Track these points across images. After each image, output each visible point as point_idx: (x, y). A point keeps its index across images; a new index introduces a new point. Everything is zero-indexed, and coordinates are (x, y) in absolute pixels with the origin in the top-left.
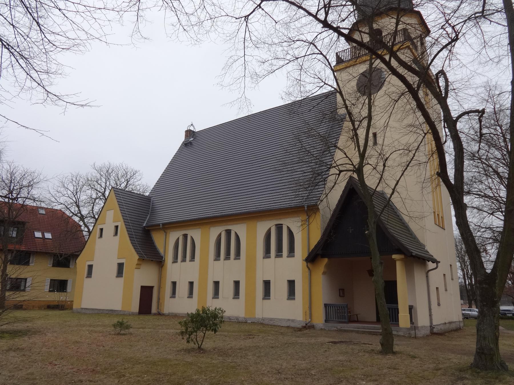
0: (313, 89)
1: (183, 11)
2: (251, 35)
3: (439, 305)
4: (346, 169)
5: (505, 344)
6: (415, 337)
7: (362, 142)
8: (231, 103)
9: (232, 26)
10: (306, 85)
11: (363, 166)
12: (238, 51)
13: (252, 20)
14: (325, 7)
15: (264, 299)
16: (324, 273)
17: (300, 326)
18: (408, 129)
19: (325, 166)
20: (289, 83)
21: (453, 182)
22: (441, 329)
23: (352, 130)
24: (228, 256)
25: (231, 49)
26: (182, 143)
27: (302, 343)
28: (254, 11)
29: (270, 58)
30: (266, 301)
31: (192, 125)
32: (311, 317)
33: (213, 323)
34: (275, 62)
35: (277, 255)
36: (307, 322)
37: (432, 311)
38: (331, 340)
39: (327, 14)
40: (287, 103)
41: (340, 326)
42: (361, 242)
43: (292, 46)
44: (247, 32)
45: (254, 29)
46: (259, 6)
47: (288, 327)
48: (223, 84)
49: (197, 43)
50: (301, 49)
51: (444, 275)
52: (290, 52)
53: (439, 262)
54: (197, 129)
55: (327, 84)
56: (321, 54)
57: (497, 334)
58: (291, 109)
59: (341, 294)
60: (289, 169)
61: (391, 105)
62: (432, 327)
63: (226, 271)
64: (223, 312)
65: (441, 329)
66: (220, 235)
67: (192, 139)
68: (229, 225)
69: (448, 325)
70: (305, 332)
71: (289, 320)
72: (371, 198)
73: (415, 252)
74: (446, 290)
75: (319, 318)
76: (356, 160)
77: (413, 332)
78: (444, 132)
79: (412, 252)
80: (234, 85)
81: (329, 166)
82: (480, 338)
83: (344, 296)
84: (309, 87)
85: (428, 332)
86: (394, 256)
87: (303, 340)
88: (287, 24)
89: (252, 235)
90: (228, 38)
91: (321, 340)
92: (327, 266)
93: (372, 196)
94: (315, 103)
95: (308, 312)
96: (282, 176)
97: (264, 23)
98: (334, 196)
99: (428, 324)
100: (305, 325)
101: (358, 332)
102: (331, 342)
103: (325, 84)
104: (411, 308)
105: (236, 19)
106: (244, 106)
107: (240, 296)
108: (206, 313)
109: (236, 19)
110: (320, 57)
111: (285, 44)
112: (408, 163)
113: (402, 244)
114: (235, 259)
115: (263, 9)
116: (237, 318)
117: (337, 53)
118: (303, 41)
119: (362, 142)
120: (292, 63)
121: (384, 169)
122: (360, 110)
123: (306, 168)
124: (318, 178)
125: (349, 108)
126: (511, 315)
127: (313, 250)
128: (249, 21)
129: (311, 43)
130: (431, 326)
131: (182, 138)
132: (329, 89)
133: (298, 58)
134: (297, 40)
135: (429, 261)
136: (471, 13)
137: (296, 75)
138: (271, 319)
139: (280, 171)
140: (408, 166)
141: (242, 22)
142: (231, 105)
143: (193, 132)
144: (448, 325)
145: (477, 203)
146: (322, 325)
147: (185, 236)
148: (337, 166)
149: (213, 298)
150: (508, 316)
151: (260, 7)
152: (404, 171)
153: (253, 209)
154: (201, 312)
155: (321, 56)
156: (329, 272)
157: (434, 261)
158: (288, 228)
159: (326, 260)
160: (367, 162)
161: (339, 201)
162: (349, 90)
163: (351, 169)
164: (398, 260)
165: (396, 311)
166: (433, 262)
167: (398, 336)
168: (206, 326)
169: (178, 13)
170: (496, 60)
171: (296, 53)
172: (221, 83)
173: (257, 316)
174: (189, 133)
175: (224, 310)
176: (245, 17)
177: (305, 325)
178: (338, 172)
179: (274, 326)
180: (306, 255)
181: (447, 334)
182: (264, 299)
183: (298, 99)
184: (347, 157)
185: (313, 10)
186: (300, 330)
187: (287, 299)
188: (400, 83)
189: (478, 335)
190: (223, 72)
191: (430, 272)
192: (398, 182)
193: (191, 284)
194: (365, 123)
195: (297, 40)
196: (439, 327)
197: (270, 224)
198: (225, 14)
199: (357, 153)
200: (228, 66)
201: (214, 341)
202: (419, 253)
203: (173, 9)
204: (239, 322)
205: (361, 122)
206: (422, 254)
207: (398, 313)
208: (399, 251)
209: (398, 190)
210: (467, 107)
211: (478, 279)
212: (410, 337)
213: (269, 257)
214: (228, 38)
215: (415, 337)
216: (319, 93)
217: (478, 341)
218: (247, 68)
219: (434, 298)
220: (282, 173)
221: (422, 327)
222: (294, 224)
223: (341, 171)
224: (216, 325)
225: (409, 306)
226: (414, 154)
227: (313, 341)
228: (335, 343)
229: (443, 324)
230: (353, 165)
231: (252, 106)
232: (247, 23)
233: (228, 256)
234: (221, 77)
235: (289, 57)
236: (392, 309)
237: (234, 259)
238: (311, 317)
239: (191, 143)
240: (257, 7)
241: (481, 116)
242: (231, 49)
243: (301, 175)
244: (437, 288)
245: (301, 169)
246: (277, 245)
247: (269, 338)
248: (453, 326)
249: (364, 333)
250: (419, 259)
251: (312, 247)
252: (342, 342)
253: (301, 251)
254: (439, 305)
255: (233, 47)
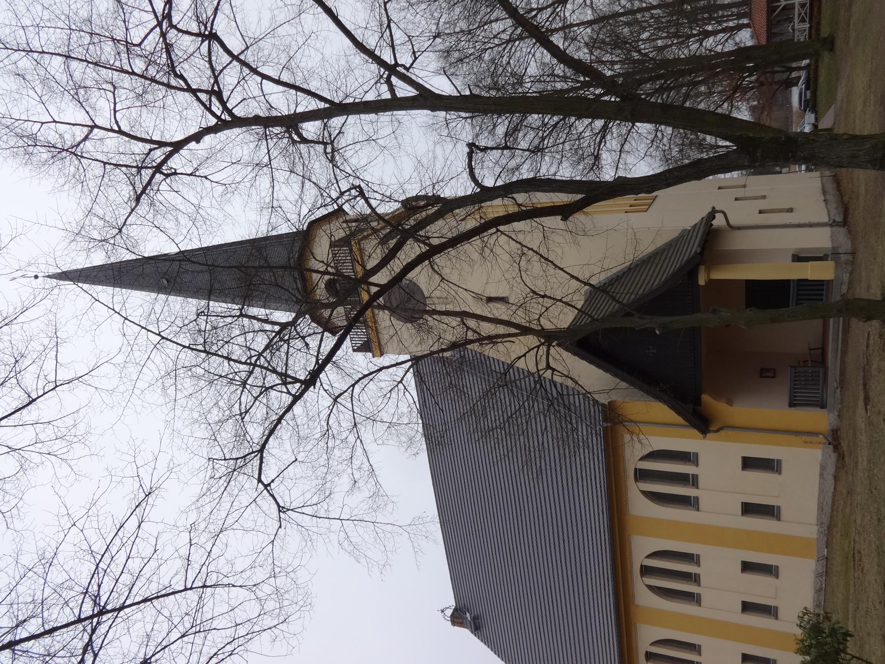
0: (405, 404)
1: (255, 620)
2: (309, 503)
3: (791, 210)
4: (544, 356)
5: (862, 111)
6: (853, 253)
7: (501, 330)
8: (416, 552)
9: (292, 537)
10: (400, 412)
11: (543, 329)
12: (333, 529)
13: (287, 499)
14: (285, 383)
15: (778, 518)
16: (730, 403)
17: (833, 457)
18: (487, 254)
19: (537, 392)
20: (391, 442)
21: (579, 197)
22: (836, 208)
23: (481, 344)
24: (694, 578)
25: (327, 540)
26: (472, 636)
27: (869, 461)
28: (273, 496)
29: (349, 470)
30: (784, 514)
31: (442, 611)
32: (816, 434)
33: (830, 635)
34: (356, 463)
35: (693, 485)
36: (824, 441)
37: (803, 221)
38: (861, 403)
39: (296, 380)
40: (425, 446)
41: (832, 383)
42: (677, 336)
43: (335, 432)
44: (304, 510)
45: (301, 499)
46: (266, 486)
47: (836, 478)
48: (382, 563)
49: (309, 600)
50: (343, 418)
51: (736, 199)
52: (344, 435)
53: (714, 208)
54: (451, 602)
55: (402, 379)
56: (353, 385)
57: (845, 137)
58: (436, 441)
59: (771, 374)
60: (537, 455)
61: (447, 288)
62: (833, 224)
63: (722, 582)
64: (806, 612)
65: (836, 208)
66: (650, 587)
67: (468, 615)
68: (632, 567)
69: (828, 197)
70: (845, 448)
71: (821, 475)
72: (597, 320)
73: (696, 248)
74: (764, 197)
75: (819, 419)
76: (532, 340)
77: (843, 258)
78: (496, 207)
79: (696, 253)
80: (387, 544)
81: (538, 386)
82: (854, 162)
83: (775, 370)
84: (404, 408)
85: (842, 231)
86: (702, 282)
87: (863, 456)
88: (300, 439)
89: (654, 528)
90: (309, 543)
91: (861, 423)
92: (716, 396)
93: (593, 319)
94: (430, 401)
95: (804, 438)
96: (548, 467)
97: (294, 481)
98: (588, 376)
99: (827, 231)
100: (831, 447)
101: (844, 353)
102: (866, 405)
103: (401, 382)
104: (798, 258)
105: (280, 527)
106: (424, 530)
107: (774, 564)
108: (810, 646)
109: (280, 527)
110: (357, 389)
111: (330, 444)
112: (543, 260)
113: (681, 268)
114: (698, 564)
115: (273, 481)
116: (818, 575)
117: (354, 350)
118: (329, 415)
119: (501, 330)
120: (362, 433)
121: (550, 298)
122: (451, 330)
123: (539, 426)
124: (558, 400)
125: (443, 347)
126: (808, 93)
127: (686, 420)
128: (287, 506)
129: (335, 400)
130: (831, 226)
131: (464, 634)
132: (410, 375)
133: (355, 424)
134: (328, 424)
135: (712, 225)
136: (323, 159)
137: (381, 428)
138: (821, 509)
139: (540, 472)
140: (547, 259)
141: (287, 518)
142: (419, 552)
143: (455, 610)
144: (828, 197)
145: (614, 143)
146: (831, 415)
147: (646, 571)
148: (538, 371)
149: (777, 618)
150: (811, 97)
151: (269, 485)
152: (556, 266)
153: (604, 520)
154: (808, 658)
155: (356, 386)
156: (728, 395)
157: (712, 215)
158: (643, 459)
159: (706, 398)
160: (535, 322)
161: (599, 366)
162: (415, 342)
163: (545, 350)
164: (708, 275)
165: (803, 284)
166: (714, 218)
167: (851, 282)
168: (838, 652)
169: (256, 628)
170: (396, 124)
171: (347, 424)
172: (381, 567)
173: (815, 536)
174: (457, 618)
175: (802, 609)
176: (280, 511)
177: (831, 447)
178: (550, 371)
179: (833, 504)
180: (695, 432)
181: (846, 199)
182: (778, 518)
183: (420, 429)
184: (524, 355)
185: (288, 399)
186: (841, 457)
187: (780, 473)
188: (418, 269)
189: (847, 167)
190: (363, 561)
191: (731, 223)
192: (573, 277)
193: (747, 567)
194: (472, 323)
195: (328, 424)
196: (833, 212)
197: (634, 491)
198: (271, 545)
199: (521, 338)
200: (356, 552)
201: (869, 634)
202: (697, 242)
203: (249, 636)
204: (826, 573)
205: (468, 328)
206: (700, 235)
207: (806, 280)
208: (692, 274)
209: (587, 276)
210: (461, 163)
211: (746, 164)
212: (853, 263)
213: (697, 499)
214: (309, 543)
215: (853, 253)
216: (414, 393)
217: (859, 166)
218: (360, 517)
219: (781, 220)
220: (543, 468)
221: (833, 241)
222: (634, 453)
223: (548, 367)
224: (833, 631)
225: (793, 261)
226: (529, 249)
227: (863, 438)
228: (867, 400)
229: (826, 204)
230: (538, 347)
231: (424, 515)
232: (288, 510)
233: (694, 578)
234: (370, 565)
235: (352, 439)
236: (798, 295)
237: (699, 565)
238: (816, 434)
239: (475, 618)
240: (268, 491)
241: (478, 147)
242: (327, 540)
243: (550, 435)
244: (761, 212)
245: (540, 434)
246: (675, 484)
247: (858, 522)
248: (830, 187)
249: (845, 342)
250: (708, 240)
251: (680, 420)
252: (865, 385)
253: (687, 441)
254: (791, 210)
255: (324, 536)
